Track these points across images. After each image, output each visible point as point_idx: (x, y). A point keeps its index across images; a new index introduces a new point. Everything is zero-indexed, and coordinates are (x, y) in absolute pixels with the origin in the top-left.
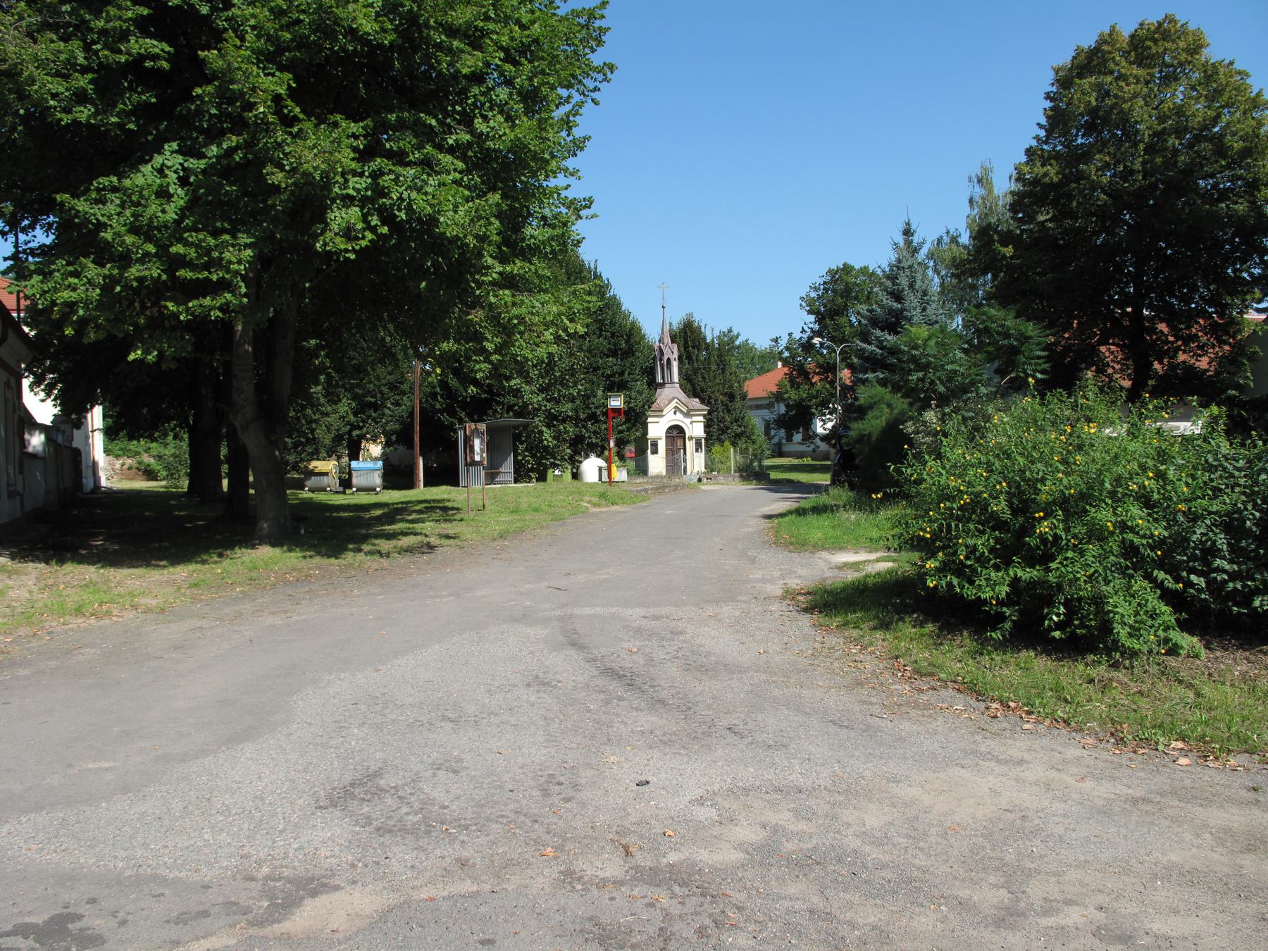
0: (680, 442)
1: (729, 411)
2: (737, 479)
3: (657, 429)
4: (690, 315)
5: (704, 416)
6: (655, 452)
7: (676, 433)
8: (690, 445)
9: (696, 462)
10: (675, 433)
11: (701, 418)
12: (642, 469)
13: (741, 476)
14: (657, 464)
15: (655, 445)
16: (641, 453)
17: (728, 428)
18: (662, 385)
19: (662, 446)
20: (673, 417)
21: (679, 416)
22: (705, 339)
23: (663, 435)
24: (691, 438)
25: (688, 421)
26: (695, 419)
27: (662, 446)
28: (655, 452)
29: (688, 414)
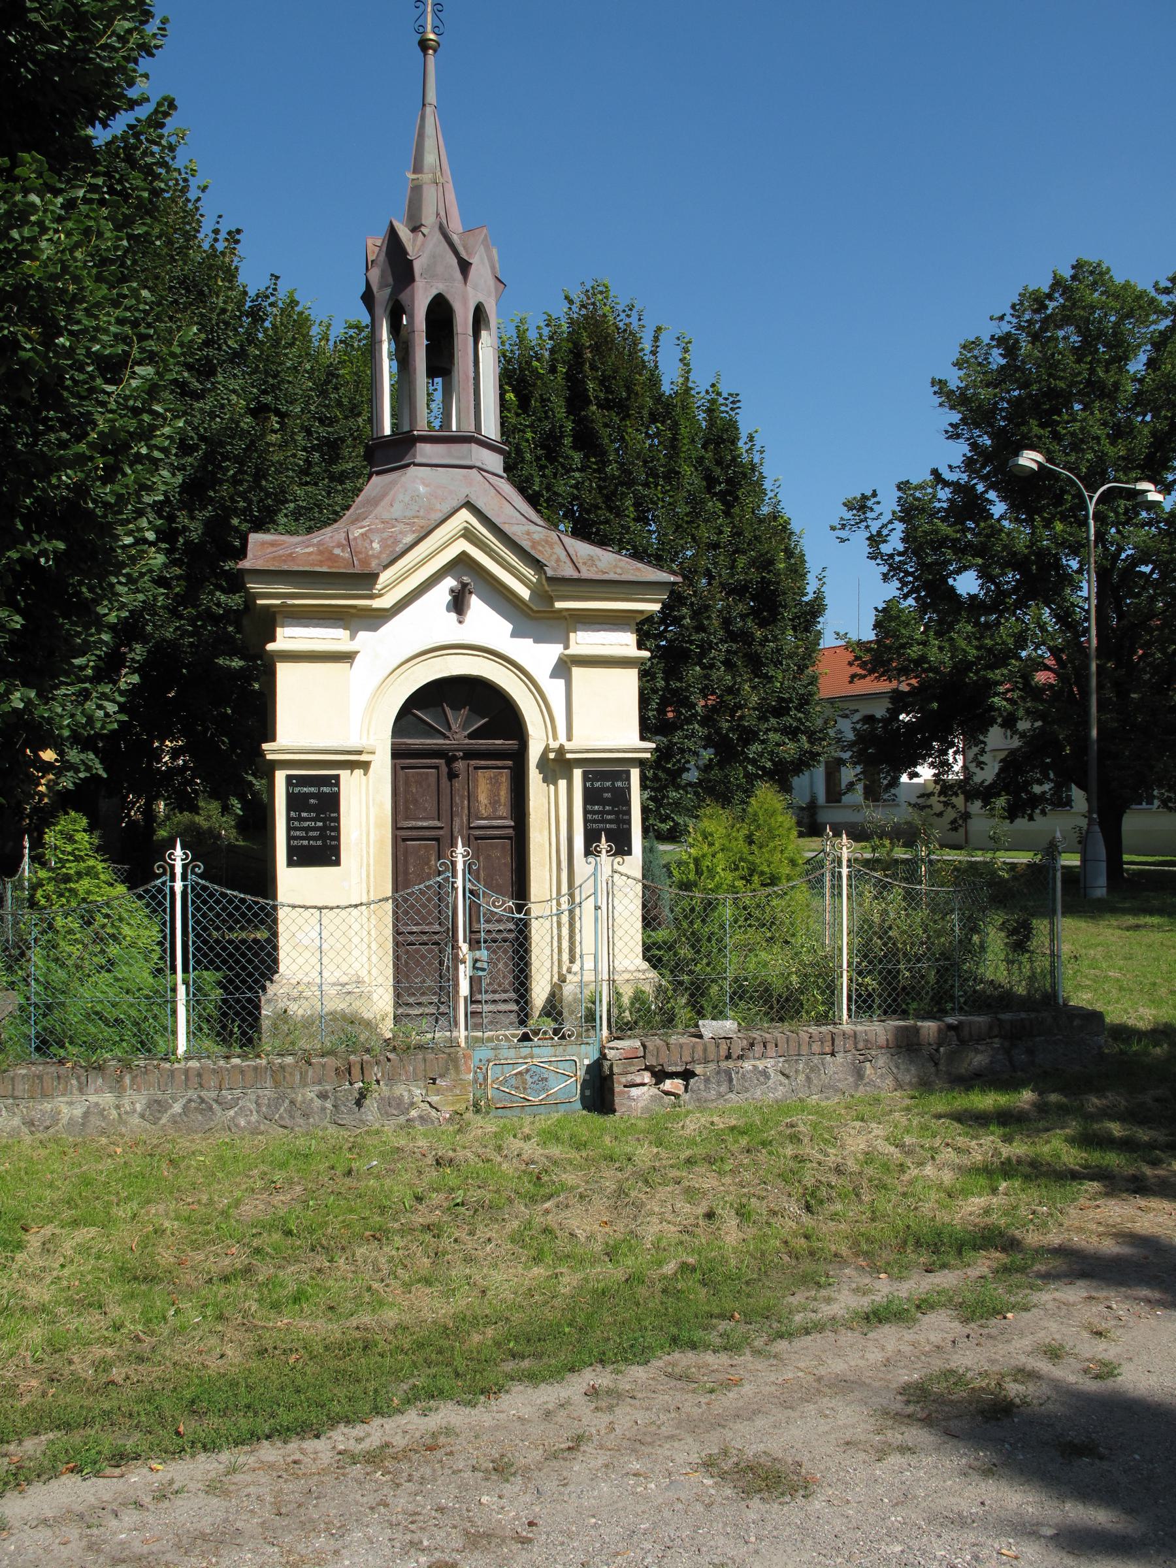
0: (487, 790)
1: (755, 663)
2: (880, 1073)
3: (334, 702)
4: (598, 291)
5: (645, 629)
6: (320, 850)
7: (461, 733)
8: (553, 809)
9: (593, 921)
10: (459, 730)
11: (624, 643)
12: (239, 962)
13: (906, 1046)
14: (333, 932)
15: (318, 802)
16: (242, 878)
17: (748, 736)
18: (395, 452)
19: (366, 809)
20: (447, 628)
21: (485, 623)
22: (654, 381)
23: (376, 737)
24: (558, 765)
25: (540, 656)
26: (585, 642)
27: (366, 809)
28: (320, 850)
29: (536, 617)
